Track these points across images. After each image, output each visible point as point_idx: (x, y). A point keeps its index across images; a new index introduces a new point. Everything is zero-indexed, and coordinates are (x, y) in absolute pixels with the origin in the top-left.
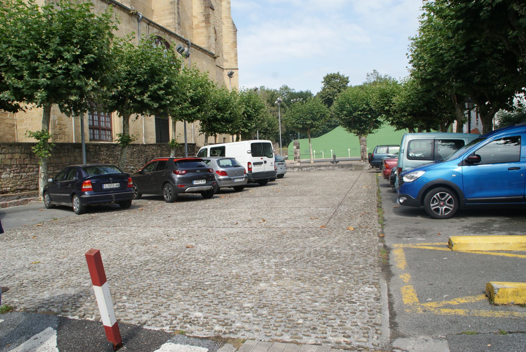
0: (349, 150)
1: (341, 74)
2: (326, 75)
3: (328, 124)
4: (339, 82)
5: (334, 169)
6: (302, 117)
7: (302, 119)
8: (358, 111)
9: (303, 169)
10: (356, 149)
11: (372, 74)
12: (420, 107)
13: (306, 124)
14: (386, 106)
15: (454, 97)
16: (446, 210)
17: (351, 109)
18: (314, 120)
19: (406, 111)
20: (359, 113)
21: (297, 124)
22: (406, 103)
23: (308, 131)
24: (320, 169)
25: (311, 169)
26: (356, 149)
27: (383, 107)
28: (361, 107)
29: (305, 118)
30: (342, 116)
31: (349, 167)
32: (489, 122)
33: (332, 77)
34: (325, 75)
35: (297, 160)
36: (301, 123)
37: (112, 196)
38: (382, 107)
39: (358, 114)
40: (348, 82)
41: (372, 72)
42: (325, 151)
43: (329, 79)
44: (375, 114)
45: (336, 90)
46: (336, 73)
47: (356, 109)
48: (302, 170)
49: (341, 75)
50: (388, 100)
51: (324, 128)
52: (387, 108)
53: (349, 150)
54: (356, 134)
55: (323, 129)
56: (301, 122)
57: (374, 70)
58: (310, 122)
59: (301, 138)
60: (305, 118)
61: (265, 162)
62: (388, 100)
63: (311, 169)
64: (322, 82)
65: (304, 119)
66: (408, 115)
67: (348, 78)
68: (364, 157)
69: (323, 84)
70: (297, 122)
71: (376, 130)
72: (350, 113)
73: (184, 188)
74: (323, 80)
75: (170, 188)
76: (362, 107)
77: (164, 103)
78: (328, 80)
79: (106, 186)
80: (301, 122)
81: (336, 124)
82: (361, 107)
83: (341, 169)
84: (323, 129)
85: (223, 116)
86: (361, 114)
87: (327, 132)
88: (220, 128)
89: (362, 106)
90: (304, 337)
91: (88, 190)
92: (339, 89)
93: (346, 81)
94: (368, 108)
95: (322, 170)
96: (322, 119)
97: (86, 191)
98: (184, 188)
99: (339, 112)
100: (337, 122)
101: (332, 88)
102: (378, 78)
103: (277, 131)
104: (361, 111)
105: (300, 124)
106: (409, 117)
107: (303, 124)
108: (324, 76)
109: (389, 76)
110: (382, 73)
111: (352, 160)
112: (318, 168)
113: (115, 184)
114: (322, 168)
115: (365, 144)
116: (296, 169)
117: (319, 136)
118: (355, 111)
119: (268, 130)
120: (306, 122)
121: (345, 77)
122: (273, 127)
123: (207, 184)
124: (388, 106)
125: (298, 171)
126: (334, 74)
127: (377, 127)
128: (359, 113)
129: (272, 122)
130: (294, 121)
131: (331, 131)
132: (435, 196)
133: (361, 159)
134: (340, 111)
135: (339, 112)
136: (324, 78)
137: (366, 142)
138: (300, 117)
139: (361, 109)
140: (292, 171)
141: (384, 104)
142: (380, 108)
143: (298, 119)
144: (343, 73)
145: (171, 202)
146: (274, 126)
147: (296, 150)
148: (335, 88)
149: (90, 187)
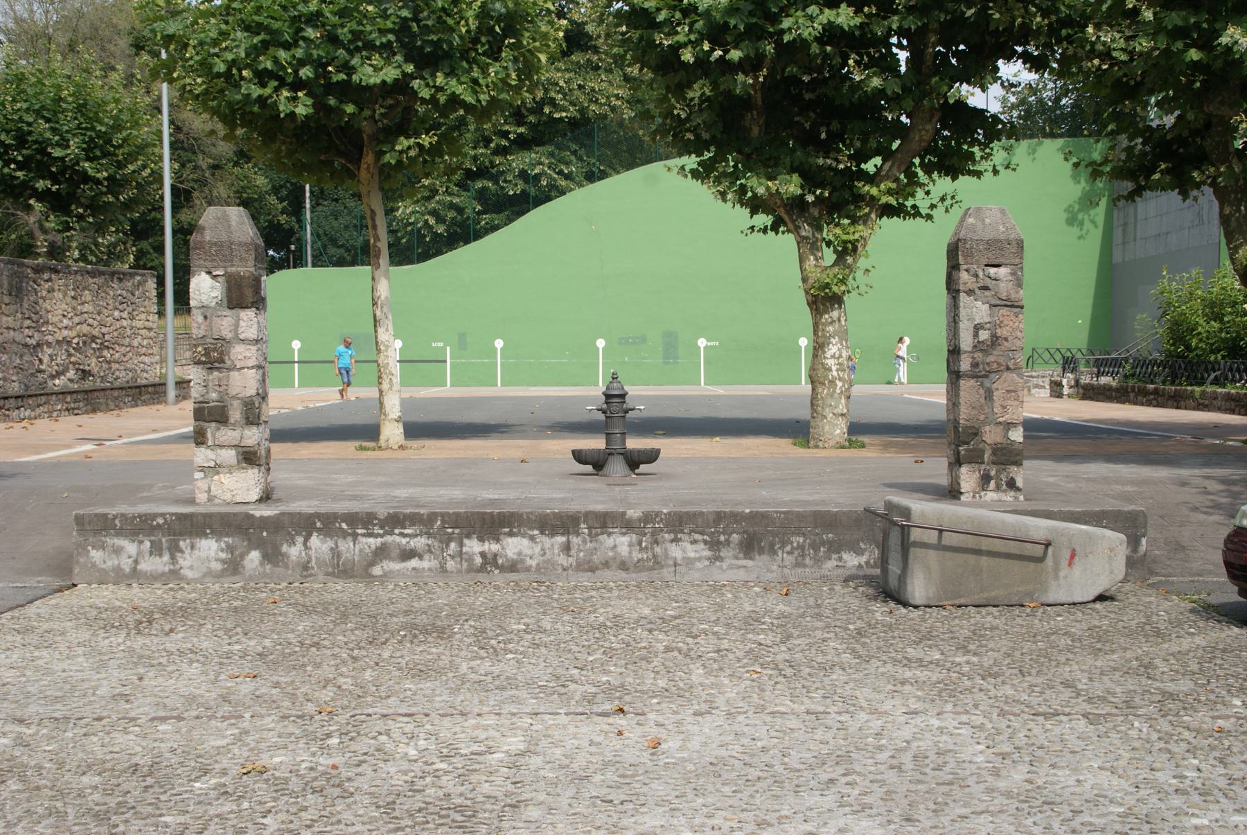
0: (601, 343)
3: (484, 189)
5: (657, 563)
7: (311, 33)
9: (294, 551)
10: (643, 340)
13: (348, 90)
18: (428, 60)
23: (369, 158)
24: (490, 561)
25: (381, 553)
26: (643, 340)
31: (836, 548)
35: (228, 435)
36: (306, 72)
42: (462, 342)
48: (273, 556)
51: (460, 210)
53: (601, 343)
54: (763, 219)
55: (451, 214)
56: (302, 63)
58: (390, 74)
59: (314, 265)
63: (381, 553)
65: (333, 39)
71: (942, 185)
80: (302, 63)
81: (532, 191)
84: (451, 214)
87: (478, 236)
95: (513, 567)
96: (494, 54)
100: (537, 178)
103: (236, 261)
105: (297, 85)
107: (320, 89)
112: (474, 546)
114: (513, 546)
116: (210, 549)
117: (425, 256)
119: (86, 178)
120: (348, 69)
122: (120, 165)
125: (233, 566)
129: (117, 127)
131: (495, 228)
137: (1017, 269)
140: (159, 564)
143: (274, 41)
146: (131, 157)
147: (224, 324)
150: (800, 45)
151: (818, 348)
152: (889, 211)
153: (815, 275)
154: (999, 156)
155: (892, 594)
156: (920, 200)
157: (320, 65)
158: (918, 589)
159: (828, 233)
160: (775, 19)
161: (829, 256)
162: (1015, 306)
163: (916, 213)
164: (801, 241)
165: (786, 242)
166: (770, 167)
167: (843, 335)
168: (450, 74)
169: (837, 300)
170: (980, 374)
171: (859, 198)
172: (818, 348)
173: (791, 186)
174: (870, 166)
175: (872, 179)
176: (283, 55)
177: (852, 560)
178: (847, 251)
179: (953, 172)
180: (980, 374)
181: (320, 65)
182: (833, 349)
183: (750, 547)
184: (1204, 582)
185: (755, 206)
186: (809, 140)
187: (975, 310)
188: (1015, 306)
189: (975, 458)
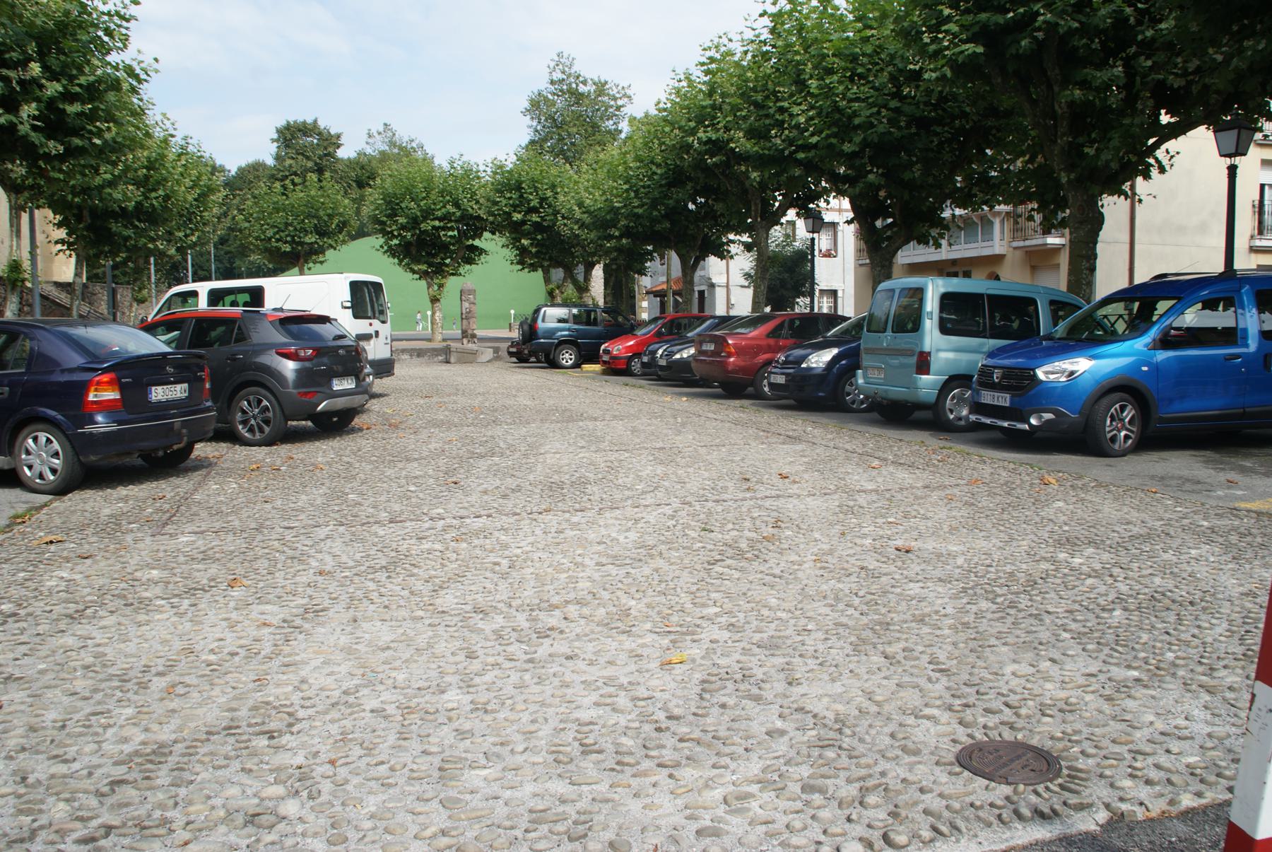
1: (322, 124)
2: (284, 123)
4: (317, 144)
6: (291, 225)
7: (291, 228)
8: (432, 220)
11: (380, 133)
12: (654, 221)
13: (302, 244)
14: (514, 211)
15: (756, 204)
16: (1126, 437)
17: (419, 214)
19: (615, 226)
20: (437, 223)
21: (278, 240)
22: (622, 207)
27: (509, 214)
28: (440, 209)
29: (298, 227)
30: (394, 227)
31: (437, 355)
32: (887, 263)
33: (300, 130)
34: (281, 123)
36: (289, 239)
37: (177, 426)
38: (505, 213)
39: (434, 227)
40: (338, 147)
41: (381, 129)
43: (290, 135)
44: (474, 226)
45: (310, 164)
46: (309, 120)
47: (427, 214)
49: (322, 127)
50: (521, 196)
52: (517, 217)
54: (418, 276)
56: (287, 236)
57: (385, 124)
60: (298, 227)
61: (377, 333)
62: (521, 196)
64: (273, 141)
65: (296, 229)
66: (621, 237)
67: (338, 136)
68: (470, 332)
69: (276, 144)
70: (277, 236)
71: (467, 267)
72: (414, 222)
73: (314, 400)
74: (275, 136)
75: (265, 403)
76: (443, 210)
77: (77, 141)
78: (289, 136)
79: (159, 394)
80: (287, 236)
82: (440, 209)
83: (416, 360)
85: (142, 205)
86: (439, 227)
88: (127, 238)
89: (444, 207)
90: (500, 775)
91: (103, 406)
92: (318, 161)
93: (331, 142)
94: (458, 214)
97: (100, 411)
98: (314, 400)
99: (385, 219)
101: (300, 157)
102: (392, 144)
104: (440, 219)
105: (286, 242)
106: (624, 241)
108: (279, 126)
109: (417, 142)
110: (404, 133)
111: (407, 340)
113: (179, 387)
115: (472, 300)
118: (425, 218)
121: (332, 133)
123: (359, 389)
124: (520, 212)
126: (304, 123)
127: (470, 261)
128: (437, 223)
130: (270, 233)
132: (1113, 410)
133: (460, 337)
134: (388, 216)
135: (385, 219)
136: (279, 131)
137: (474, 296)
138: (287, 225)
139: (439, 214)
141: (511, 206)
142: (499, 215)
143: (280, 231)
144: (329, 122)
145: (266, 446)
148: (308, 158)
149: (111, 395)
150: (426, 231)
151: (433, 314)
152: (453, 274)
153: (431, 292)
154: (483, 260)
155: (448, 362)
156: (461, 270)
157: (293, 237)
158: (452, 360)
159: (436, 281)
160: (419, 224)
161: (436, 287)
162: (474, 304)
163: (460, 274)
164: (428, 283)
165: (423, 283)
166: (418, 262)
167: (440, 310)
168: (329, 238)
169: (438, 300)
170: (467, 318)
171: (443, 271)
172: (433, 314)
173: (424, 267)
174: (448, 261)
175: (447, 265)
176: (282, 234)
177: (440, 358)
178: (441, 286)
179: (470, 263)
180: (467, 318)
181: (293, 237)
182: (438, 314)
183: (419, 356)
184: (1129, 667)
185: (414, 272)
186: (429, 254)
187: (466, 305)
188: (474, 304)
189: (466, 337)
